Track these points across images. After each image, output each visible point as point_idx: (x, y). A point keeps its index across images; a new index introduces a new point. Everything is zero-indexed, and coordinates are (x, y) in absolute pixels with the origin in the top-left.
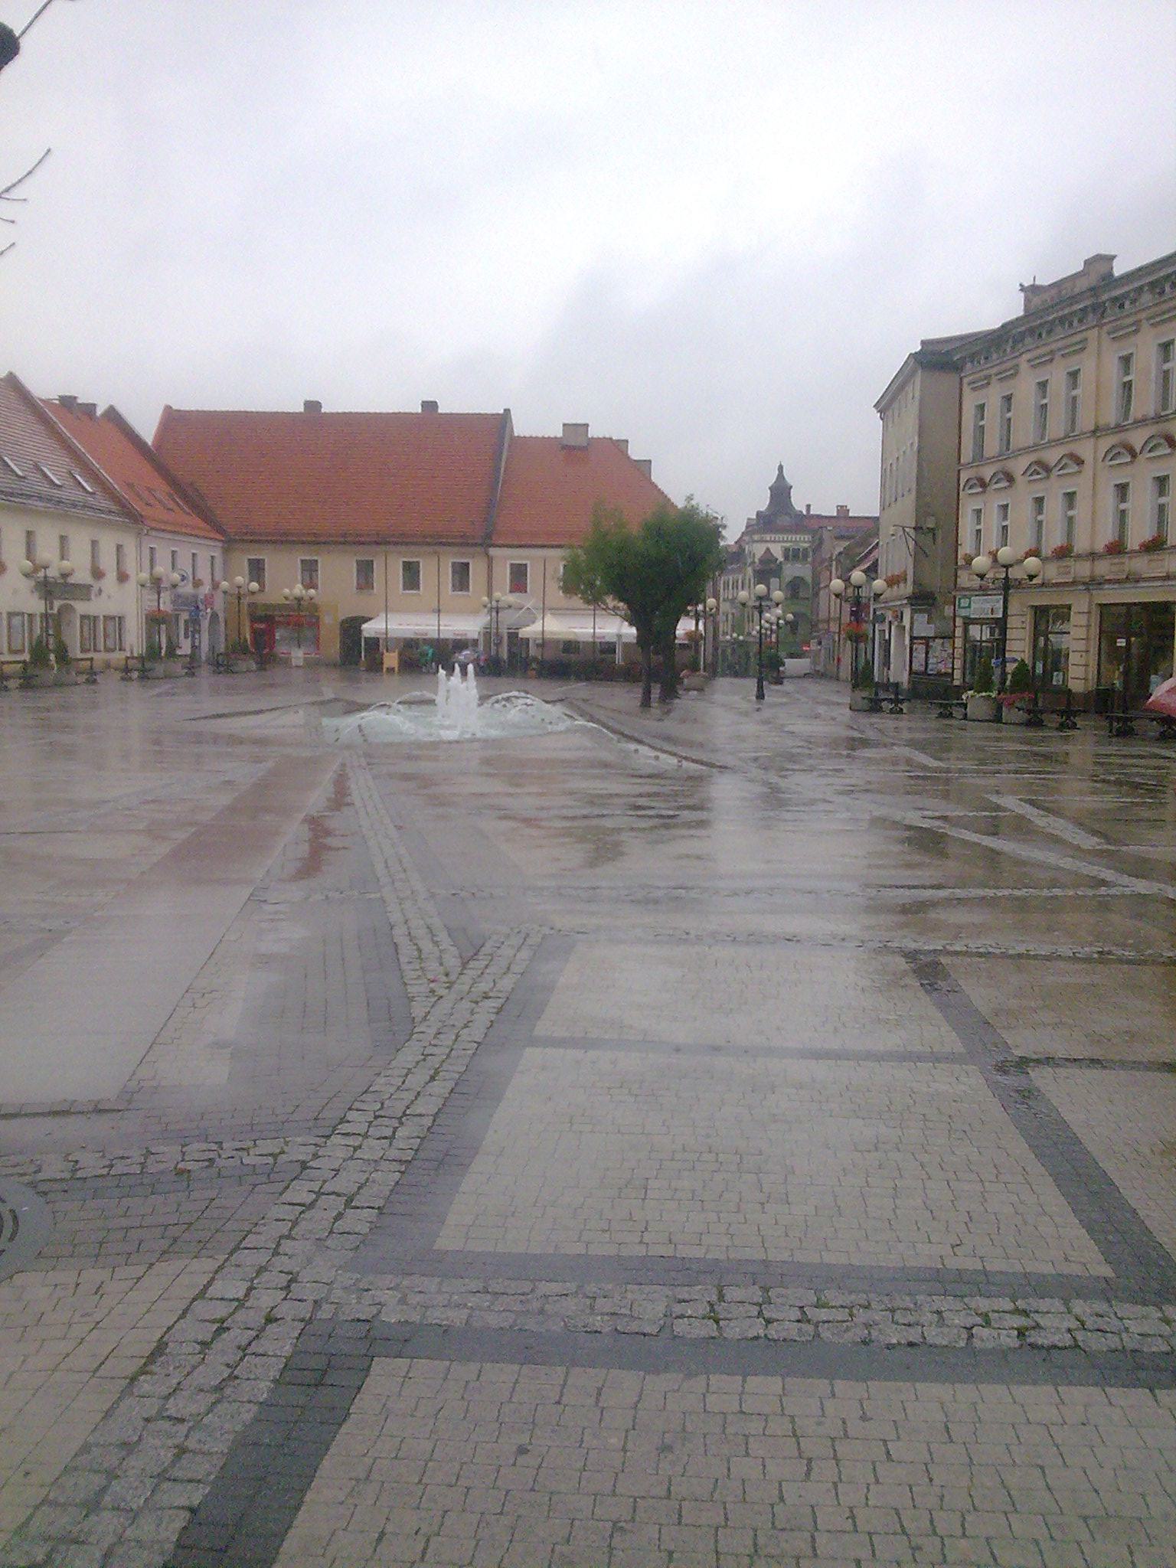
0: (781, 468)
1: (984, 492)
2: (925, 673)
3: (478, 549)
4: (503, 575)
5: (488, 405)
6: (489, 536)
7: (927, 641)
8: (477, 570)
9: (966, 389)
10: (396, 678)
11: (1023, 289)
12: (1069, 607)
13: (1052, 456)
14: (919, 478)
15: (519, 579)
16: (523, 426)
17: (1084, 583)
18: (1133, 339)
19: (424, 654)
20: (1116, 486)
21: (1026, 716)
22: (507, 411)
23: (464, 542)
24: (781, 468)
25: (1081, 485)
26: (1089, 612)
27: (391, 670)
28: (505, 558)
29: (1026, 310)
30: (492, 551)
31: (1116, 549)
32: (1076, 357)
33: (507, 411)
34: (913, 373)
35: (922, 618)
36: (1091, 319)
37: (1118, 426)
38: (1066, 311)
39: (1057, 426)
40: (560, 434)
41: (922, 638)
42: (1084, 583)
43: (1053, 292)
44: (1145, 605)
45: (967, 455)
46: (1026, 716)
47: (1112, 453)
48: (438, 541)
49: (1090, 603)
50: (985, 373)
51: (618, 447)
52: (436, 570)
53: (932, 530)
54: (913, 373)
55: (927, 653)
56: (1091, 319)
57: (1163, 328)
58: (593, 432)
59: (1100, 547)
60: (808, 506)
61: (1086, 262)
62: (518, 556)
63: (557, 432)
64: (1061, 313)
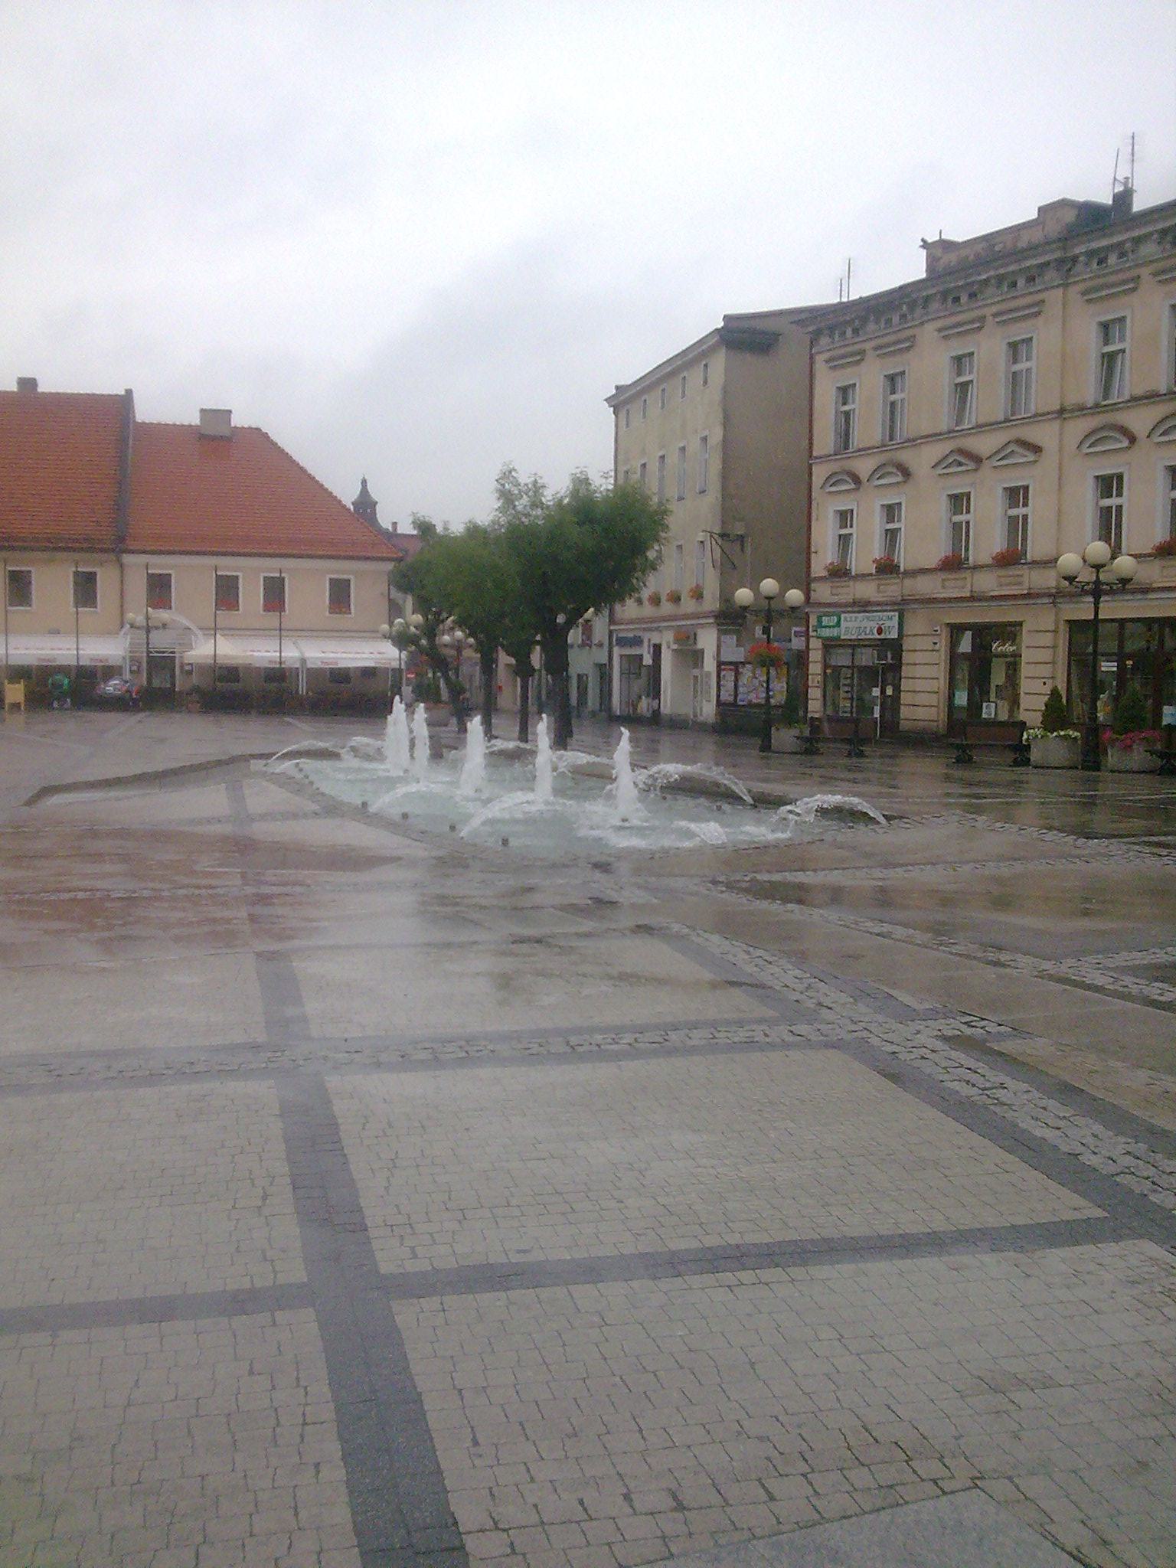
0: (364, 482)
1: (1128, 448)
2: (734, 704)
3: (112, 556)
4: (138, 587)
5: (104, 383)
6: (122, 539)
7: (736, 666)
8: (106, 580)
9: (820, 366)
10: (20, 718)
11: (925, 245)
12: (1020, 624)
13: (984, 444)
14: (725, 477)
15: (159, 589)
16: (145, 412)
17: (1050, 595)
18: (1125, 299)
19: (58, 686)
20: (1097, 477)
21: (1159, 762)
22: (129, 392)
23: (87, 545)
24: (364, 482)
25: (1038, 478)
26: (1055, 631)
27: (16, 706)
28: (138, 566)
29: (930, 268)
30: (127, 559)
31: (953, 564)
32: (1030, 323)
33: (129, 392)
34: (712, 349)
35: (731, 640)
36: (1051, 275)
37: (1097, 406)
38: (1011, 268)
39: (989, 402)
40: (198, 422)
41: (731, 663)
42: (1050, 595)
43: (984, 245)
44: (1149, 622)
45: (825, 440)
46: (1159, 762)
47: (1094, 437)
48: (55, 545)
49: (1057, 622)
50: (857, 347)
51: (257, 439)
52: (52, 582)
53: (741, 539)
54: (712, 349)
55: (736, 680)
56: (1051, 275)
57: (838, 373)
58: (237, 421)
59: (933, 562)
60: (395, 524)
61: (1042, 210)
62: (160, 564)
63: (195, 420)
64: (1002, 271)
